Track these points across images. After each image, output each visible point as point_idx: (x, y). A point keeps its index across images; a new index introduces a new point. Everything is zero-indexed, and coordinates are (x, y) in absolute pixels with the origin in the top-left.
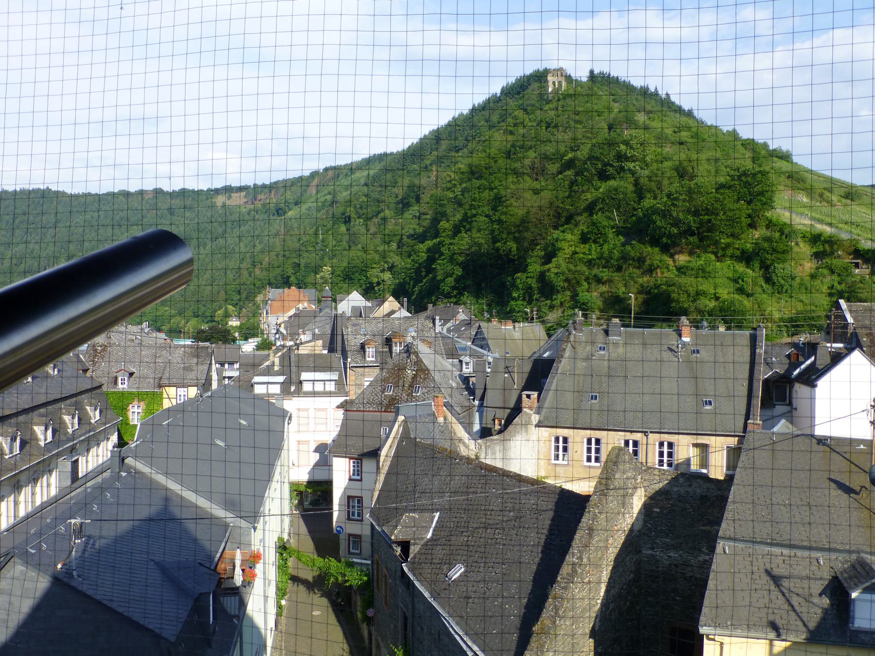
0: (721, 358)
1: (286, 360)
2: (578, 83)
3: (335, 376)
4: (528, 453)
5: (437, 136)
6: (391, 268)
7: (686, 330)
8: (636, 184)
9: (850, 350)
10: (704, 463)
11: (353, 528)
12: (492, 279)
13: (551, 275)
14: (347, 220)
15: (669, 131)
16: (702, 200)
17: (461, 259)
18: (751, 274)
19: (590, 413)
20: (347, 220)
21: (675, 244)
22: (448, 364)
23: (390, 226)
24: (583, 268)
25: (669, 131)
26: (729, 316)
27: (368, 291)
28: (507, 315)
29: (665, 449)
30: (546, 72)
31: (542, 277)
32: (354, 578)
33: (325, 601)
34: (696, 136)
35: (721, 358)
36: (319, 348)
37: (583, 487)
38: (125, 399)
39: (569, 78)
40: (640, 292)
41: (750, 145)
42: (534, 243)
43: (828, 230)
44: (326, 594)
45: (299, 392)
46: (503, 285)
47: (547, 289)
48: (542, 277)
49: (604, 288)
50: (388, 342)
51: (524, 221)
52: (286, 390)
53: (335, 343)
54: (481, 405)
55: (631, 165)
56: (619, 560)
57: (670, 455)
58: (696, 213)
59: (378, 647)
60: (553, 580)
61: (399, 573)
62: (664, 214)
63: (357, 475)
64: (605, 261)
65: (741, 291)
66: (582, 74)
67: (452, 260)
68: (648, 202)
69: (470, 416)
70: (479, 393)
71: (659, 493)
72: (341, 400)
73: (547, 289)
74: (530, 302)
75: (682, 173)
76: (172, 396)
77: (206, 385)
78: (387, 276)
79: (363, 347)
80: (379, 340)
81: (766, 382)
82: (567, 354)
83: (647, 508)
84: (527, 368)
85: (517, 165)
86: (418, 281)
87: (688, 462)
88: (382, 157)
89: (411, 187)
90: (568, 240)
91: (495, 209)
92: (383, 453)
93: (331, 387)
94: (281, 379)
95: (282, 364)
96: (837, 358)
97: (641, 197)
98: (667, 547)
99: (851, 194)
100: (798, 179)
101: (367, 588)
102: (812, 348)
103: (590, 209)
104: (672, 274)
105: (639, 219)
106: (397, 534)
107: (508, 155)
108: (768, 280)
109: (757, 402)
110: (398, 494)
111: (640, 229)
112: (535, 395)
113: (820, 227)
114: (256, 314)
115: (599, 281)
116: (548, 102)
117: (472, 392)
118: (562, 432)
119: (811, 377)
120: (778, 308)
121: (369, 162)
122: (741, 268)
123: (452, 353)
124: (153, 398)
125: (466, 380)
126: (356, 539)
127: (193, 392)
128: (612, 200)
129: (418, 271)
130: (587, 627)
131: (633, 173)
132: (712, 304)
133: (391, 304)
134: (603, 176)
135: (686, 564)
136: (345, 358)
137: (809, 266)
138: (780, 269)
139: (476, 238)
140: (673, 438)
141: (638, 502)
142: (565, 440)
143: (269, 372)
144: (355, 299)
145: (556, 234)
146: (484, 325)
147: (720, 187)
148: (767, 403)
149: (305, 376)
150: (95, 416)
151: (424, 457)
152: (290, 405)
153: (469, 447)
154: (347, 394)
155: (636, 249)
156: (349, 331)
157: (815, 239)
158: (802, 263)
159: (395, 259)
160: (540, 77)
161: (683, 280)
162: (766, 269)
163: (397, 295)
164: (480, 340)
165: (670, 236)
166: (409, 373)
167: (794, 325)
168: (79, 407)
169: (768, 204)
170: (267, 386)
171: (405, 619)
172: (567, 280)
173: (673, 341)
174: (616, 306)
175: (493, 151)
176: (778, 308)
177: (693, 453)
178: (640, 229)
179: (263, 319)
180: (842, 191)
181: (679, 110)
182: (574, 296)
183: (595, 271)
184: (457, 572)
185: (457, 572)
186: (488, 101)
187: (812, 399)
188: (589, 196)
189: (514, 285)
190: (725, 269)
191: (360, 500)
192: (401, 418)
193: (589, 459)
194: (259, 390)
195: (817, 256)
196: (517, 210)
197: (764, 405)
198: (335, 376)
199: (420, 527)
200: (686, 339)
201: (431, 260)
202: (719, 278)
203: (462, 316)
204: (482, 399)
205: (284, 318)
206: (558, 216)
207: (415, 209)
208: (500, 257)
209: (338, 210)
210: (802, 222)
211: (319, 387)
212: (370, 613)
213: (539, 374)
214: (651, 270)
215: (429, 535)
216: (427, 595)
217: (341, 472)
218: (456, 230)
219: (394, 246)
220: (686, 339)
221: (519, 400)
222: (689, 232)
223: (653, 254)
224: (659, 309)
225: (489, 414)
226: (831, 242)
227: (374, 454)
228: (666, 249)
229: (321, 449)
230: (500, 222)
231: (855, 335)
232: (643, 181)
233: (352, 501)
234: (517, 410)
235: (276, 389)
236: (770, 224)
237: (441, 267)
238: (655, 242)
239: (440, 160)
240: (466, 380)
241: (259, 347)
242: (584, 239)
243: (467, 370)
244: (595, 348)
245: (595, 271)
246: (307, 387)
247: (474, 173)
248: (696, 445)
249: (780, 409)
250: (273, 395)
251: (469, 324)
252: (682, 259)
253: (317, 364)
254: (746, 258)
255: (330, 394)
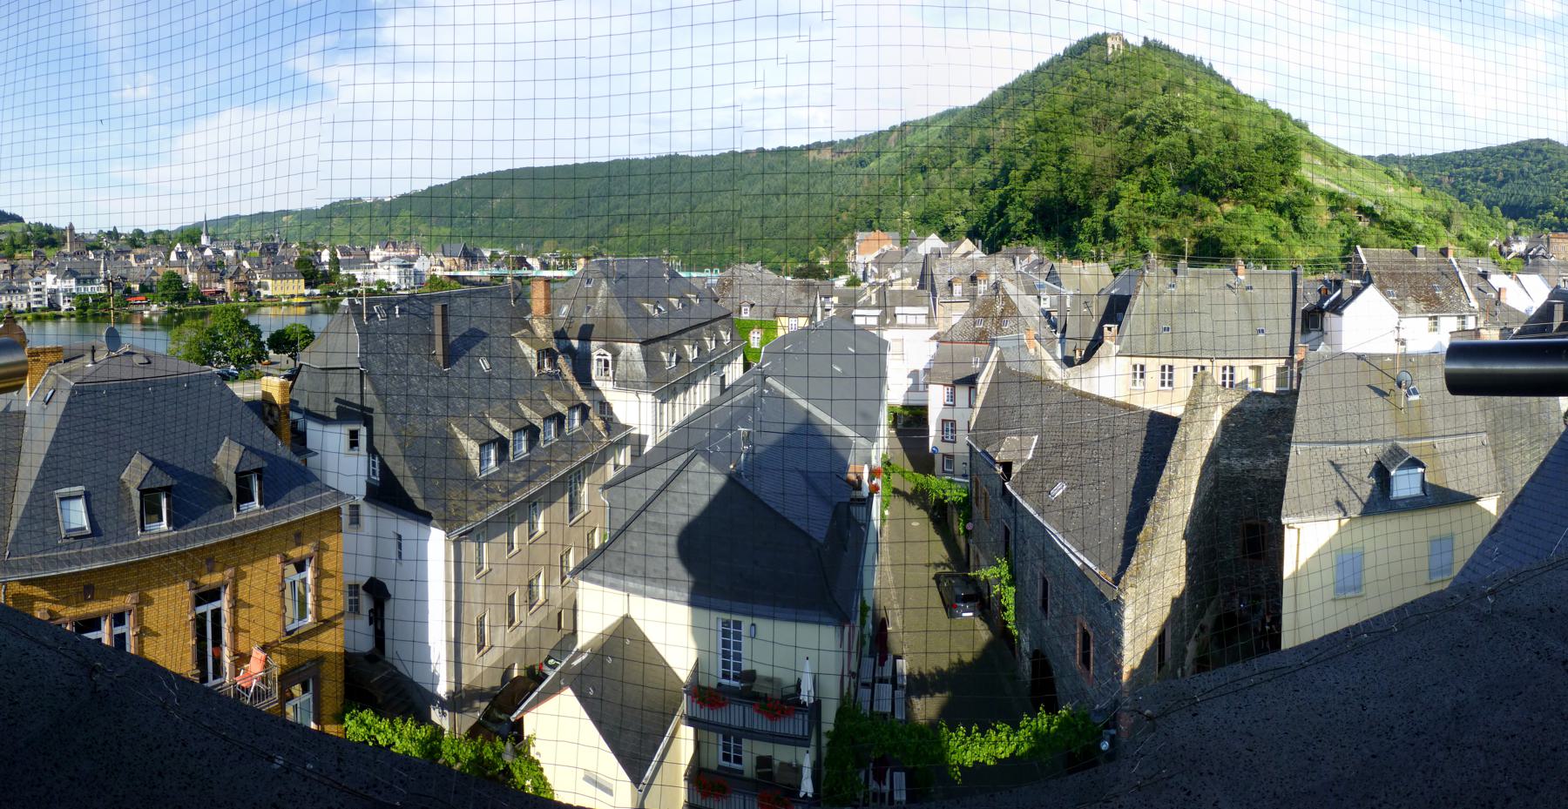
0: (1269, 294)
1: (882, 292)
2: (1138, 49)
3: (925, 310)
4: (1109, 377)
5: (1006, 91)
6: (965, 213)
7: (1241, 269)
8: (1190, 141)
9: (1366, 286)
10: (1259, 381)
11: (946, 448)
12: (1061, 223)
13: (1115, 221)
14: (924, 170)
15: (1214, 96)
16: (1242, 160)
17: (1032, 204)
18: (1284, 224)
19: (1169, 343)
20: (924, 170)
21: (1222, 196)
22: (1031, 299)
23: (963, 174)
24: (1142, 214)
25: (1214, 96)
26: (1266, 257)
27: (945, 233)
28: (1075, 256)
29: (1228, 373)
30: (1105, 36)
31: (1106, 222)
32: (955, 494)
33: (924, 514)
34: (1236, 102)
35: (1269, 294)
36: (909, 285)
37: (1177, 411)
38: (748, 327)
39: (1126, 43)
40: (1193, 236)
41: (1277, 114)
42: (1098, 192)
43: (1341, 190)
44: (924, 507)
45: (893, 324)
46: (1069, 229)
47: (1110, 233)
48: (1106, 222)
49: (1161, 233)
50: (973, 279)
51: (1090, 173)
52: (882, 324)
53: (925, 280)
54: (1062, 338)
55: (1186, 124)
56: (1204, 469)
57: (1232, 377)
58: (1240, 169)
59: (977, 557)
60: (1152, 493)
61: (999, 491)
62: (1214, 169)
63: (951, 403)
64: (1159, 208)
65: (1275, 236)
66: (1137, 42)
67: (1022, 205)
68: (1200, 158)
69: (1054, 347)
70: (1060, 327)
71: (1234, 410)
72: (933, 332)
73: (1110, 233)
74: (1095, 244)
75: (1228, 134)
76: (787, 325)
77: (812, 316)
78: (960, 220)
79: (950, 284)
80: (966, 278)
81: (1304, 311)
82: (1141, 291)
83: (1224, 424)
84: (1104, 302)
85: (1082, 120)
86: (990, 224)
87: (1246, 381)
88: (951, 113)
89: (982, 139)
90: (1129, 189)
91: (1062, 159)
92: (981, 380)
93: (922, 320)
94: (877, 312)
95: (878, 298)
96: (1357, 292)
97: (1194, 154)
98: (1241, 456)
99: (1351, 162)
100: (1315, 146)
101: (966, 506)
102: (1338, 284)
103: (1150, 161)
104: (1220, 222)
105: (1192, 173)
106: (1001, 457)
107: (1072, 111)
108: (1297, 228)
109: (1298, 329)
110: (994, 422)
111: (1193, 181)
112: (1114, 327)
113: (1334, 187)
114: (843, 252)
115: (1157, 226)
116: (1108, 63)
117: (1054, 326)
118: (1139, 361)
119: (1338, 307)
120: (1304, 252)
121: (941, 116)
122: (1275, 217)
123: (1032, 290)
124: (768, 327)
125: (1048, 314)
126: (949, 458)
127: (803, 322)
128: (1169, 156)
129: (990, 216)
130: (1181, 535)
131: (1187, 131)
132: (1254, 247)
133: (967, 245)
134: (1161, 132)
135: (1256, 469)
136: (935, 295)
137: (1327, 217)
138: (1308, 219)
139: (1045, 185)
140: (1234, 363)
141: (1218, 415)
142: (1142, 367)
143: (866, 306)
144: (933, 242)
145: (1119, 183)
146: (1056, 264)
147: (1259, 148)
148: (1306, 330)
149: (898, 310)
150: (726, 337)
151: (1017, 384)
152: (888, 335)
153: (1056, 372)
154: (936, 327)
155: (1189, 198)
156: (937, 270)
157: (1331, 195)
158: (1320, 215)
159: (968, 205)
160: (1099, 41)
161: (1228, 225)
162: (1294, 217)
163: (973, 235)
164: (1052, 276)
165: (1219, 188)
166: (999, 308)
167: (1317, 265)
168: (716, 332)
169: (1296, 164)
170: (865, 318)
171: (1007, 532)
172: (1129, 225)
173: (1231, 280)
174: (1172, 250)
175: (1058, 107)
176: (1304, 252)
177: (1251, 376)
178: (1193, 181)
179: (850, 258)
180: (1345, 159)
181: (1219, 78)
182: (1135, 239)
183: (1154, 217)
184: (1058, 490)
185: (1058, 490)
186: (1052, 60)
187: (1340, 324)
188: (1149, 150)
189: (1080, 228)
190: (1262, 219)
191: (953, 423)
192: (996, 349)
193: (1163, 384)
194: (859, 321)
195: (1333, 209)
196: (1083, 161)
197: (1303, 332)
198: (925, 310)
199: (1019, 449)
200: (1242, 277)
201: (1002, 205)
202: (1259, 226)
203: (1034, 257)
204: (1064, 331)
205: (871, 257)
206: (1120, 167)
207: (986, 159)
208: (1067, 203)
209: (914, 161)
210: (1321, 183)
211: (911, 320)
212: (970, 526)
213: (1116, 309)
214: (1202, 218)
215: (1030, 457)
216: (1032, 511)
217: (936, 399)
218: (1027, 178)
219: (967, 192)
220: (1242, 277)
221: (1100, 331)
222: (1234, 185)
223: (1205, 204)
224: (1210, 251)
225: (1070, 345)
226: (1341, 199)
227: (970, 381)
228: (1214, 199)
229: (914, 374)
230: (1068, 171)
231: (1368, 273)
232: (1196, 138)
233: (948, 426)
234: (1096, 343)
235: (873, 321)
236: (1297, 182)
237: (1012, 213)
238: (1206, 193)
239: (1008, 115)
240: (1048, 314)
241: (848, 284)
242: (1144, 189)
243: (1046, 305)
244: (1161, 287)
245: (1154, 217)
246: (900, 320)
247: (1040, 127)
248: (1252, 367)
249: (1314, 334)
250: (873, 327)
251: (1041, 263)
252: (1228, 208)
253: (910, 300)
254: (1280, 209)
255: (917, 326)
